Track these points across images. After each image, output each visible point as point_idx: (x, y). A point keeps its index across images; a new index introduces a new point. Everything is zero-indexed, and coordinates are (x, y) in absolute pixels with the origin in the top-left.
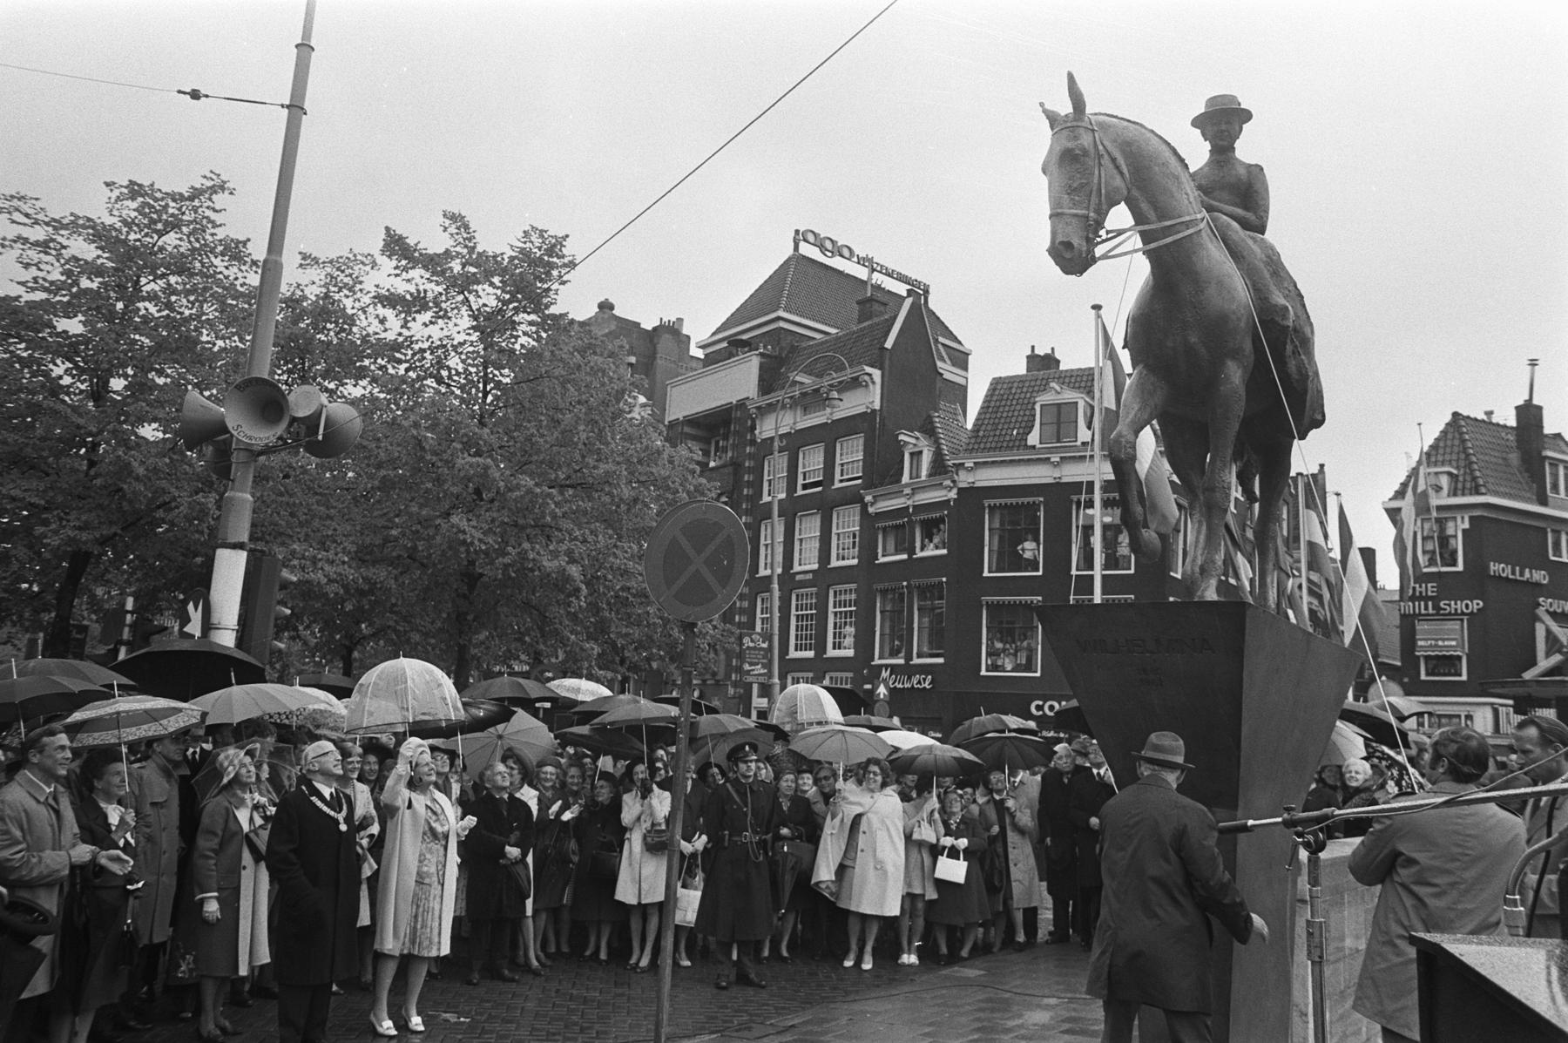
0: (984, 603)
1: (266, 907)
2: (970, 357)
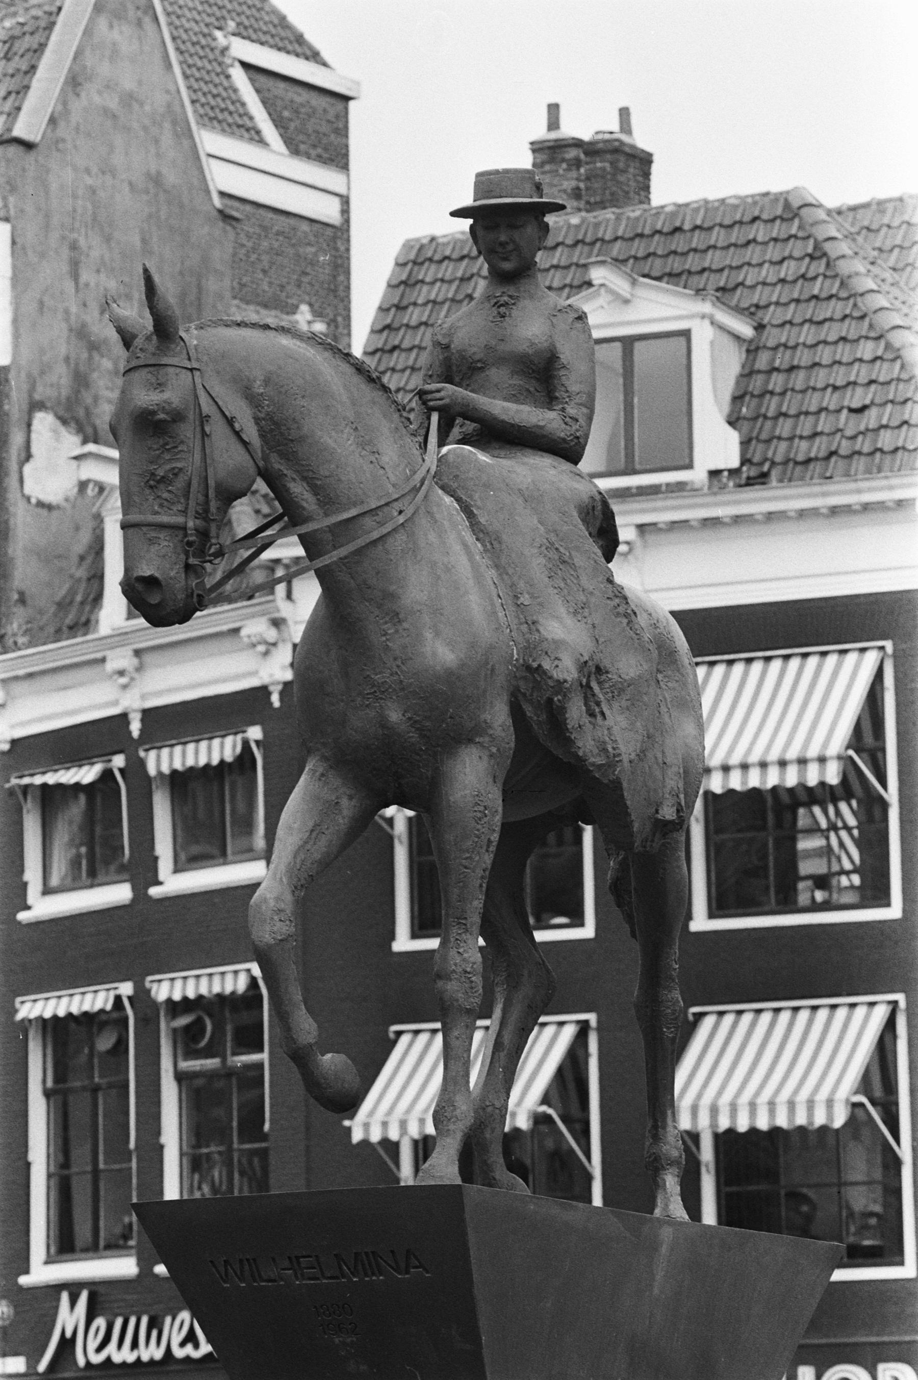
2: (352, 104)
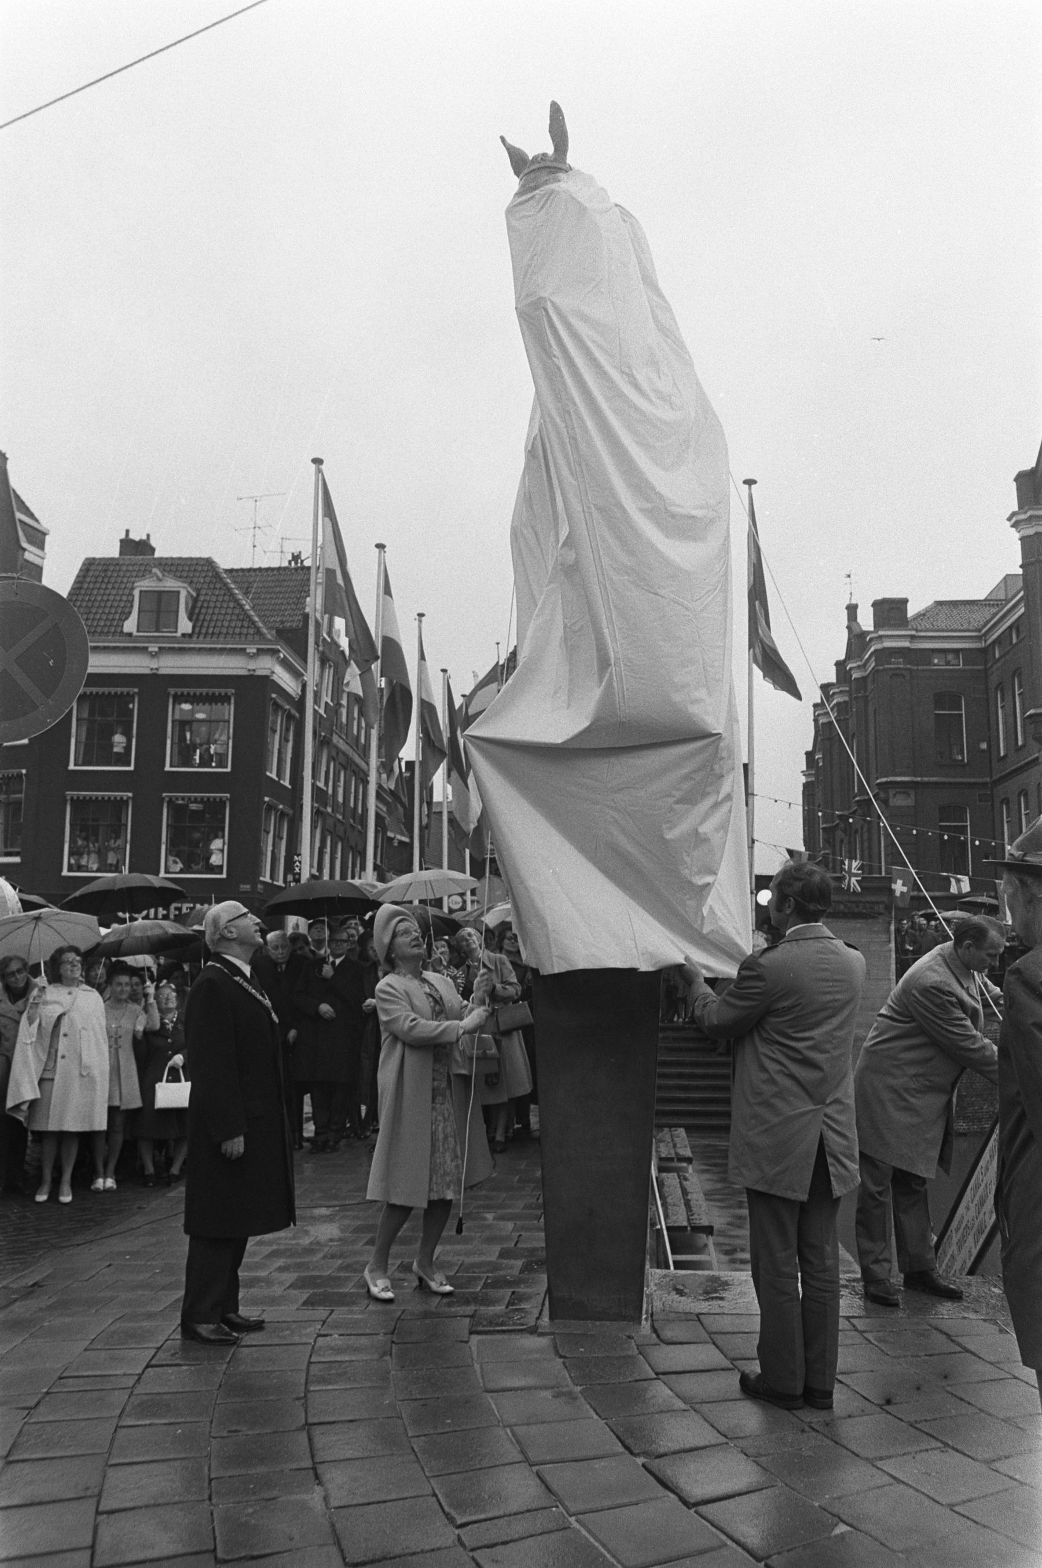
0: (68, 798)
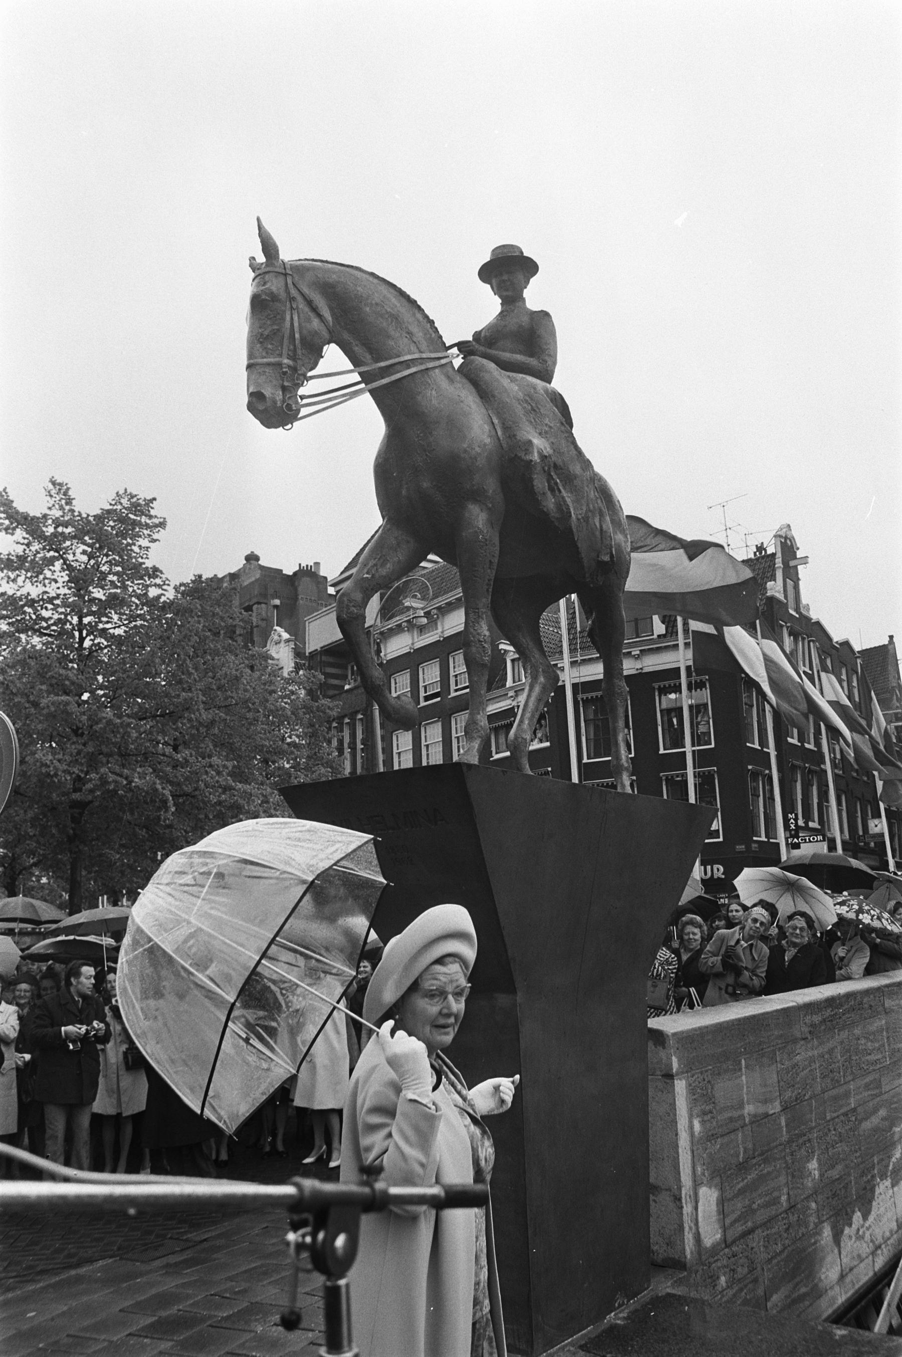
1: (722, 1020)
